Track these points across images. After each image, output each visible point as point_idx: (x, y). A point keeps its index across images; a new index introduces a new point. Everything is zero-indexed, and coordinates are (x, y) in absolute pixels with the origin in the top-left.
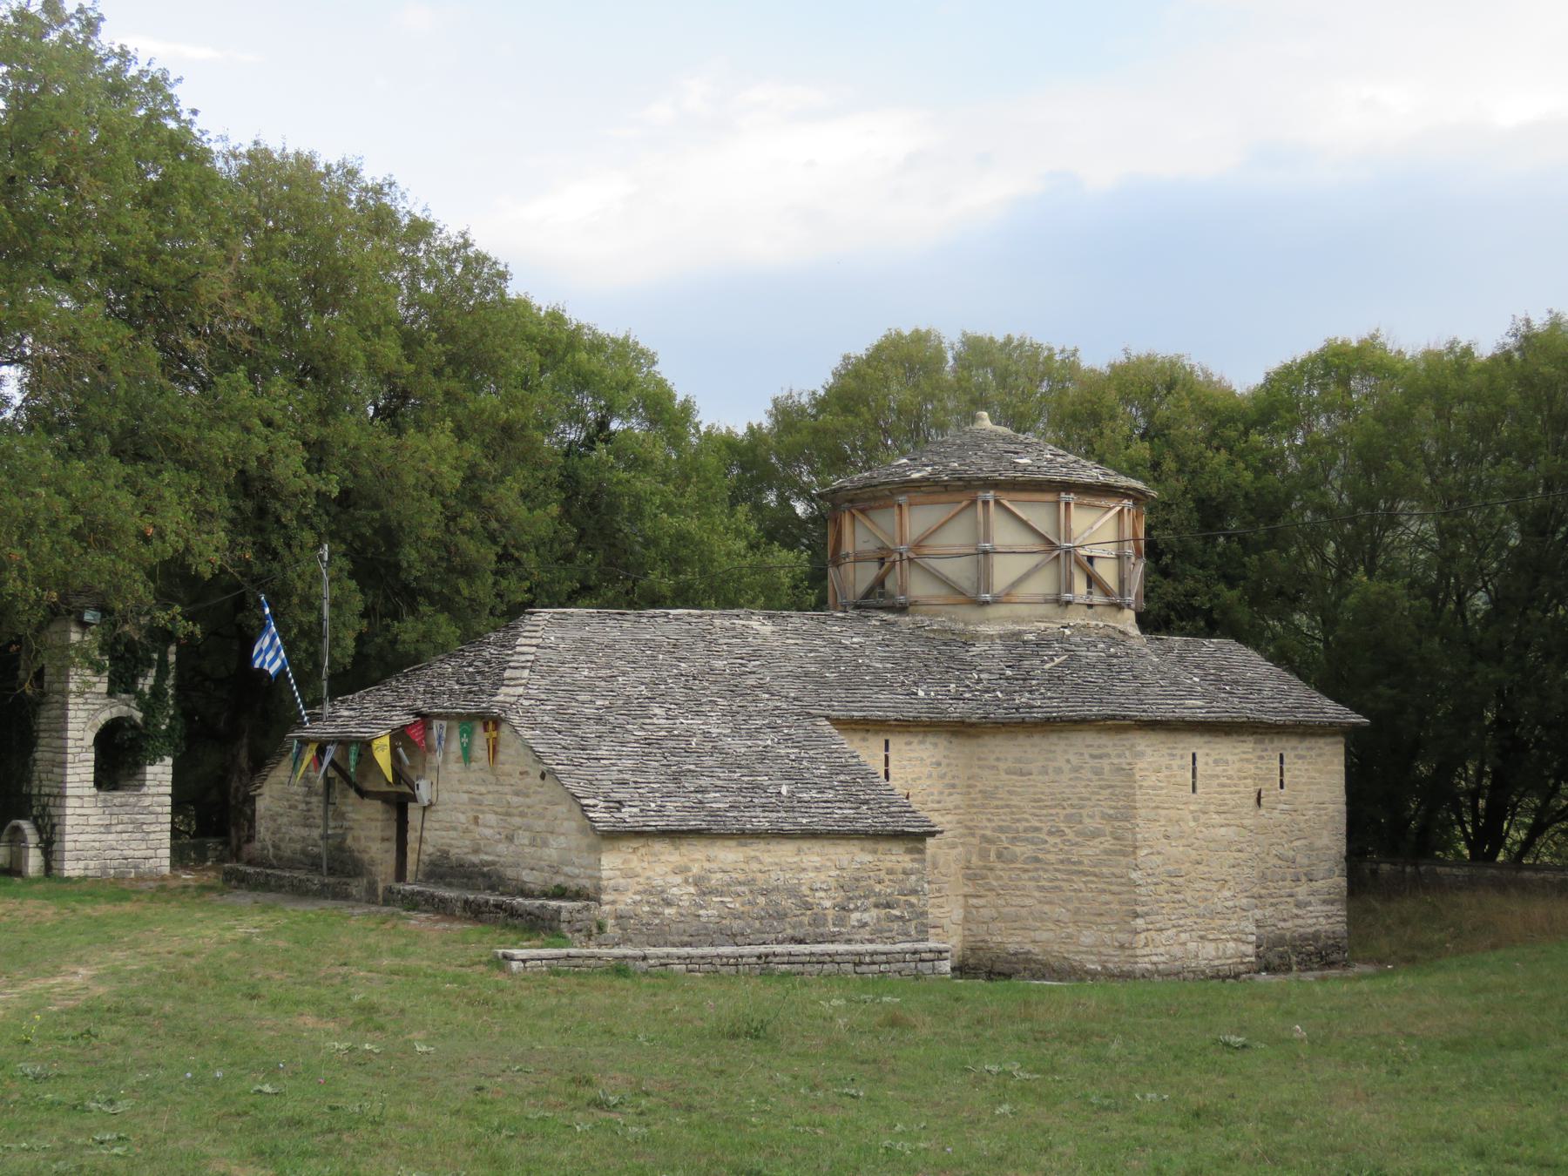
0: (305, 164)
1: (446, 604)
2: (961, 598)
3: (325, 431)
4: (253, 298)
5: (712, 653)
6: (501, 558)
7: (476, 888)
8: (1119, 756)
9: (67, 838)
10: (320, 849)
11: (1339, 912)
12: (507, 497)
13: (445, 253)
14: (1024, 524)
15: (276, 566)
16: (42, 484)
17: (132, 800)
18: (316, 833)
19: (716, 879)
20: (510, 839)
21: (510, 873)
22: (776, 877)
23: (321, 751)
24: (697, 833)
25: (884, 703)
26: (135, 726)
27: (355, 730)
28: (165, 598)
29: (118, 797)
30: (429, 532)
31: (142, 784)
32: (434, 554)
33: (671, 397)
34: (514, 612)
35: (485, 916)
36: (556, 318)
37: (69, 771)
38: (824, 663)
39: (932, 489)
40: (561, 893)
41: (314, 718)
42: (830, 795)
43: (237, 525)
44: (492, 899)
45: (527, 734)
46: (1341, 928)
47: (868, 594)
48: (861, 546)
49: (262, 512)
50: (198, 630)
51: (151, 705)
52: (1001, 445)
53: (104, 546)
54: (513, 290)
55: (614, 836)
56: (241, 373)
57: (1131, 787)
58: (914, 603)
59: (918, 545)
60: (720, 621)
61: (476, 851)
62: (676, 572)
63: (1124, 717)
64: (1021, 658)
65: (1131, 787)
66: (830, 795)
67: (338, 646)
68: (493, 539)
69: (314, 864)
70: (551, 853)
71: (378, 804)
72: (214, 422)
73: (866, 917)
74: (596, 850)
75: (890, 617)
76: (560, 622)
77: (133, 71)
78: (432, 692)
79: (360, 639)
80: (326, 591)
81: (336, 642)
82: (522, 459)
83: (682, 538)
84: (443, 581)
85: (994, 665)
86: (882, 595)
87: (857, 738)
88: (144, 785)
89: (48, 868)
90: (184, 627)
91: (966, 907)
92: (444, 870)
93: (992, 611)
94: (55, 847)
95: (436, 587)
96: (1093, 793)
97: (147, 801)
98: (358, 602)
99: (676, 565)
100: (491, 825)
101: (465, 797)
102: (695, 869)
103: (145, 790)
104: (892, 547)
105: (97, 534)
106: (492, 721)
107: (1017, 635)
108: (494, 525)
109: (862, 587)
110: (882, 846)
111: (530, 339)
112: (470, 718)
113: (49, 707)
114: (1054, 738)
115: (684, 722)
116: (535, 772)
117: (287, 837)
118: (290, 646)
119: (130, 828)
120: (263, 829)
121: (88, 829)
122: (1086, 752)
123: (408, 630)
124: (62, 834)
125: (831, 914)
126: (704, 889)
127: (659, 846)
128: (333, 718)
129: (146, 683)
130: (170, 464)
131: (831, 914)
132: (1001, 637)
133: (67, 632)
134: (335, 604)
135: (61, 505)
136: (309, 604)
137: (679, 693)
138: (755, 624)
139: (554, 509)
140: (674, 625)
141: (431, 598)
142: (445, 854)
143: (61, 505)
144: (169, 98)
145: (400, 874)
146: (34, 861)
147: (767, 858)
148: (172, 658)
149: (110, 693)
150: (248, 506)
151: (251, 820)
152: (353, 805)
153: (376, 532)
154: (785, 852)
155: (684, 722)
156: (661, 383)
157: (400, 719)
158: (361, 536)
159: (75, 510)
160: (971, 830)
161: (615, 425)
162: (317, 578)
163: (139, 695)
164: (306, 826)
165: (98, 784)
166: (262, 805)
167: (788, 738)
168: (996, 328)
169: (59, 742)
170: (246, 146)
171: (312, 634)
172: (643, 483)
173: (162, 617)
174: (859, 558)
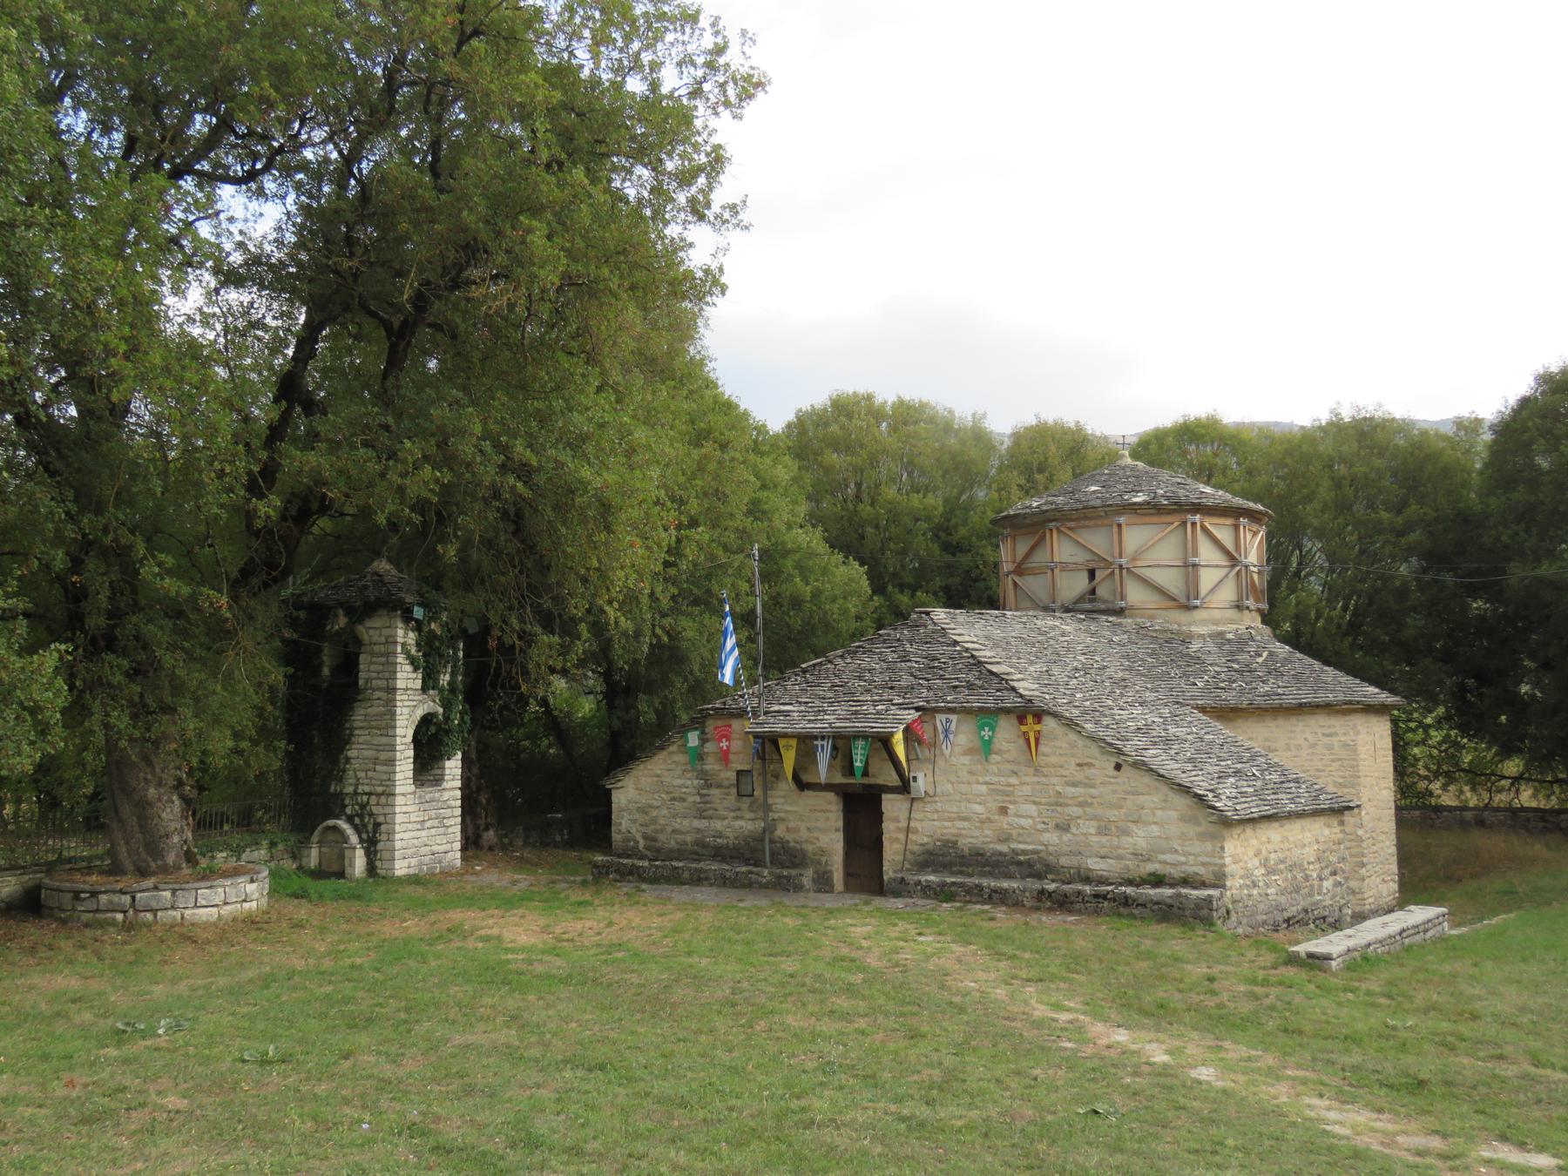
2: (1172, 603)
8: (1345, 734)
9: (397, 836)
17: (437, 795)
35: (1077, 906)
37: (398, 769)
47: (1080, 600)
57: (1355, 760)
58: (1132, 608)
63: (1358, 702)
65: (1355, 760)
70: (1139, 838)
86: (1091, 601)
88: (443, 780)
89: (371, 869)
92: (941, 857)
94: (380, 846)
96: (1327, 766)
101: (984, 788)
103: (445, 785)
104: (1111, 560)
107: (1222, 634)
113: (364, 704)
117: (669, 829)
119: (436, 822)
121: (410, 826)
122: (1320, 731)
124: (391, 833)
132: (1210, 636)
133: (392, 627)
146: (359, 862)
152: (784, 797)
164: (701, 817)
168: (913, 393)
169: (384, 740)
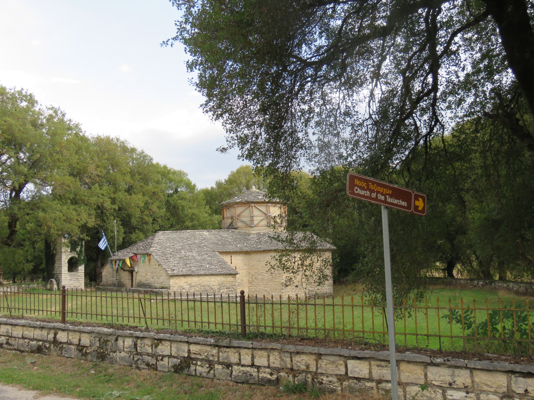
0: (108, 138)
1: (141, 230)
3: (116, 196)
4: (99, 169)
5: (195, 239)
6: (153, 220)
7: (147, 288)
10: (116, 282)
11: (331, 288)
12: (154, 208)
13: (139, 155)
14: (260, 210)
15: (105, 224)
16: (58, 211)
18: (115, 279)
19: (193, 284)
20: (153, 278)
21: (153, 285)
22: (205, 283)
23: (116, 262)
24: (189, 275)
25: (230, 248)
26: (76, 258)
27: (122, 257)
28: (82, 232)
29: (73, 273)
30: (137, 216)
31: (78, 270)
32: (139, 220)
33: (191, 183)
34: (156, 231)
36: (165, 167)
38: (219, 240)
39: (241, 204)
40: (163, 288)
41: (114, 255)
42: (217, 267)
43: (96, 217)
44: (149, 289)
45: (156, 257)
46: (332, 291)
47: (229, 226)
48: (228, 216)
49: (102, 212)
50: (89, 239)
51: (79, 254)
52: (256, 194)
53: (70, 223)
54: (154, 162)
55: (172, 276)
56: (97, 185)
59: (239, 215)
60: (197, 232)
61: (147, 281)
62: (192, 221)
64: (260, 238)
66: (217, 267)
67: (119, 239)
68: (151, 216)
69: (115, 285)
70: (161, 280)
71: (127, 272)
72: (91, 196)
73: (224, 291)
74: (169, 279)
75: (233, 230)
76: (163, 234)
77: (72, 123)
78: (137, 249)
79: (124, 238)
80: (116, 229)
81: (118, 239)
82: (157, 199)
83: (193, 214)
84: (141, 225)
85: (254, 239)
87: (225, 255)
90: (86, 238)
91: (249, 289)
92: (140, 285)
93: (254, 228)
95: (139, 227)
97: (79, 274)
98: (123, 231)
99: (192, 220)
100: (149, 276)
102: (189, 282)
105: (68, 220)
106: (149, 255)
107: (259, 233)
108: (152, 213)
109: (228, 224)
110: (227, 277)
111: (158, 173)
112: (145, 254)
114: (265, 254)
115: (188, 254)
116: (157, 264)
118: (108, 241)
120: (104, 279)
123: (133, 236)
125: (217, 290)
126: (191, 286)
127: (182, 278)
128: (117, 255)
129: (78, 249)
130: (82, 205)
131: (217, 290)
133: (61, 239)
134: (118, 231)
135: (61, 214)
136: (112, 231)
137: (187, 247)
138: (204, 233)
139: (164, 210)
140: (187, 234)
141: (138, 229)
142: (141, 282)
143: (61, 214)
144: (80, 129)
145: (132, 286)
147: (203, 280)
148: (84, 244)
149: (71, 252)
150: (99, 211)
151: (101, 277)
153: (126, 216)
154: (207, 278)
155: (188, 254)
156: (189, 180)
157: (131, 255)
158: (124, 217)
159: (64, 215)
160: (249, 273)
161: (179, 190)
162: (113, 226)
163: (77, 252)
165: (69, 271)
166: (103, 274)
167: (210, 256)
170: (96, 136)
171: (113, 238)
172: (184, 203)
173: (82, 236)
174: (227, 218)
